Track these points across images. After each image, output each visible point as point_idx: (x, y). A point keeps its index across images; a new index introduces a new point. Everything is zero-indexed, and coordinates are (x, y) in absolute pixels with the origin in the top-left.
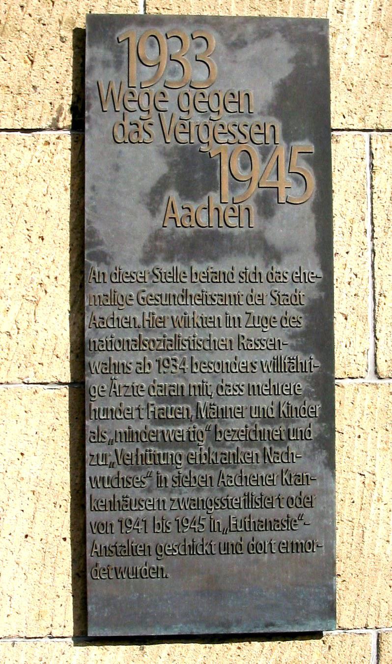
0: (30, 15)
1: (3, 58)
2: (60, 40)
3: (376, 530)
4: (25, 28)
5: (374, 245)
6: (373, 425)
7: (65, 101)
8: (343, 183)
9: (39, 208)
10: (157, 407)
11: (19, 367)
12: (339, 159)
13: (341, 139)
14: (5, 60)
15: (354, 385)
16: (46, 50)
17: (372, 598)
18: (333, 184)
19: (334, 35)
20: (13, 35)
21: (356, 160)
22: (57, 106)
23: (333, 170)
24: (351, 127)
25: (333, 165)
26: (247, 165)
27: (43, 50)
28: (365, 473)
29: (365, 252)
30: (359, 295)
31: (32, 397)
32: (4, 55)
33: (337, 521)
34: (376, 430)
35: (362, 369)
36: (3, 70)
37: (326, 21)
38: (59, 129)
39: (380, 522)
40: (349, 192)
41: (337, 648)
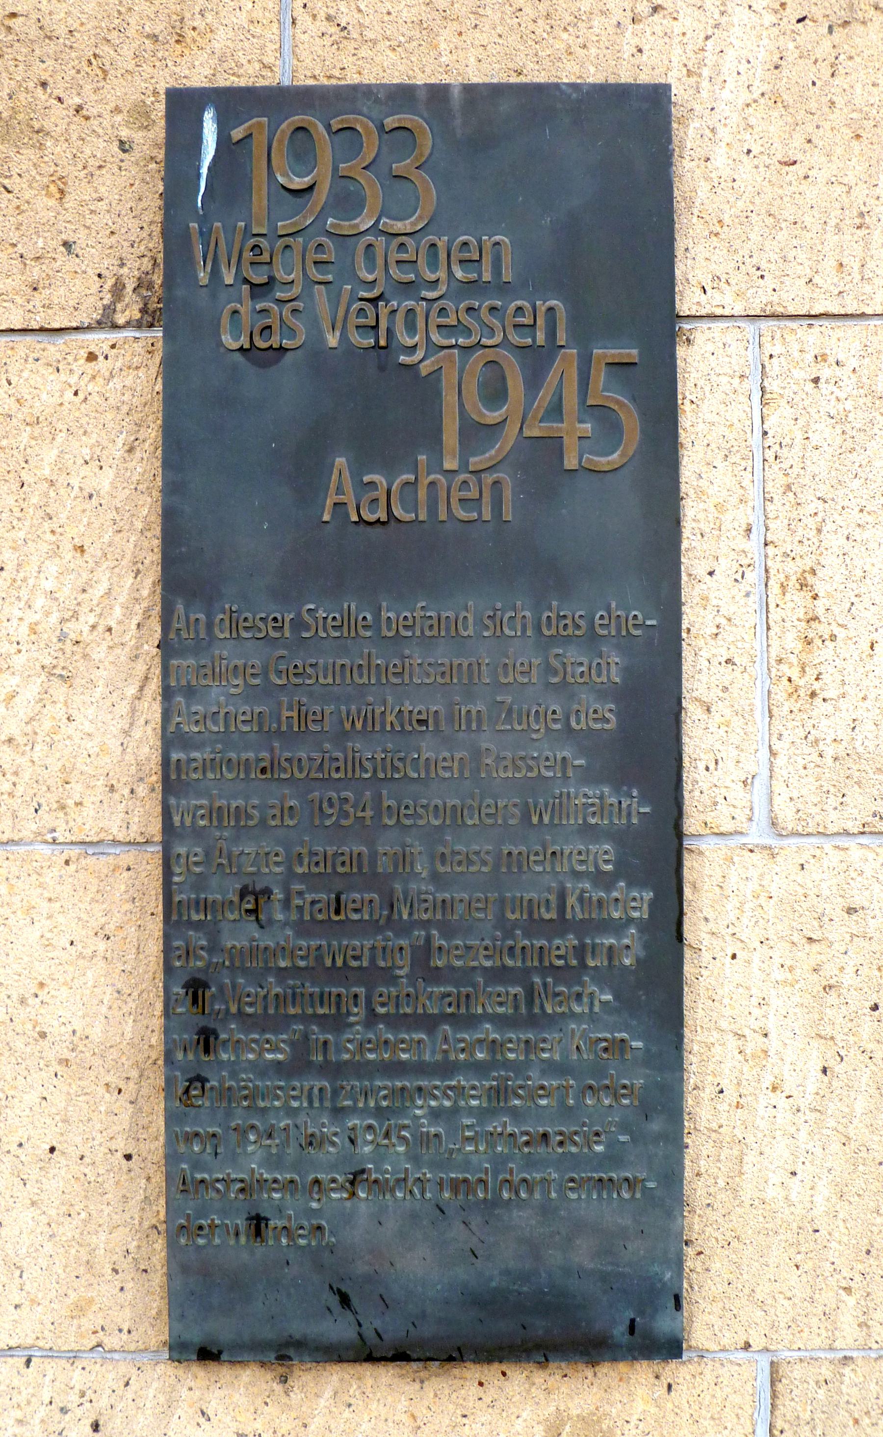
0: (60, 100)
1: (5, 188)
2: (119, 148)
3: (767, 1150)
4: (48, 125)
5: (766, 556)
6: (763, 932)
7: (125, 271)
8: (701, 427)
9: (76, 488)
10: (309, 897)
11: (36, 811)
12: (690, 384)
13: (699, 338)
14: (9, 192)
15: (725, 850)
16: (90, 169)
17: (758, 1290)
18: (681, 431)
19: (159, 1313)
20: (26, 140)
21: (728, 379)
22: (110, 282)
23: (680, 402)
24: (719, 311)
25: (679, 390)
26: (495, 393)
27: (84, 168)
28: (747, 1032)
29: (748, 572)
30: (736, 660)
31: (63, 872)
32: (6, 182)
33: (686, 1131)
34: (772, 943)
35: (741, 816)
36: (5, 212)
37: (667, 87)
38: (115, 327)
39: (778, 1133)
40: (713, 446)
41: (685, 1388)
